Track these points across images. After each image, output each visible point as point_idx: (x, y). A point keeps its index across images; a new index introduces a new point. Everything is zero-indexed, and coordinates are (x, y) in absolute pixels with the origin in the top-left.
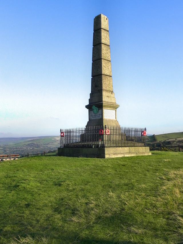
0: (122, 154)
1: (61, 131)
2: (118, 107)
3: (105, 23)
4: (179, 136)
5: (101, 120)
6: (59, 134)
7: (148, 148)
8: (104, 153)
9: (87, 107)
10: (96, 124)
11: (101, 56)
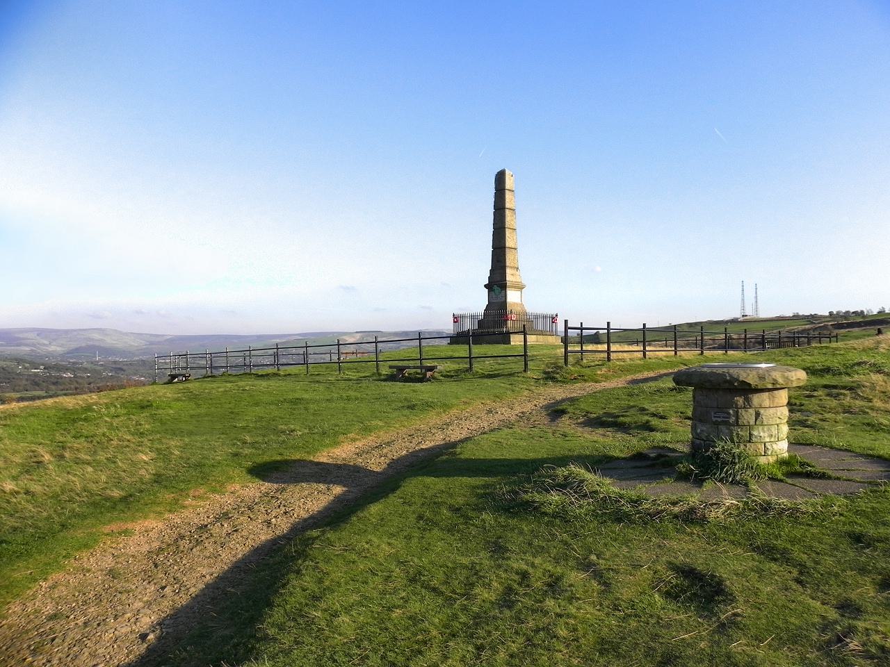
1: (454, 315)
4: (658, 336)
5: (504, 304)
9: (485, 286)
10: (497, 308)
11: (505, 225)
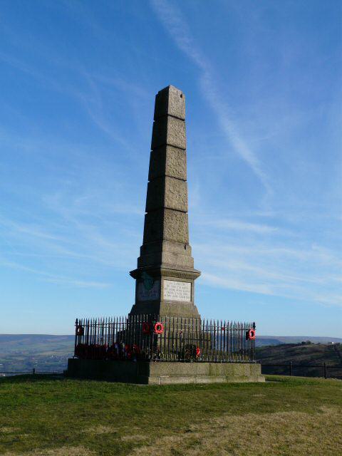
0: (190, 376)
1: (77, 323)
2: (196, 277)
3: (175, 106)
6: (72, 331)
7: (258, 368)
8: (147, 374)
9: (133, 274)
